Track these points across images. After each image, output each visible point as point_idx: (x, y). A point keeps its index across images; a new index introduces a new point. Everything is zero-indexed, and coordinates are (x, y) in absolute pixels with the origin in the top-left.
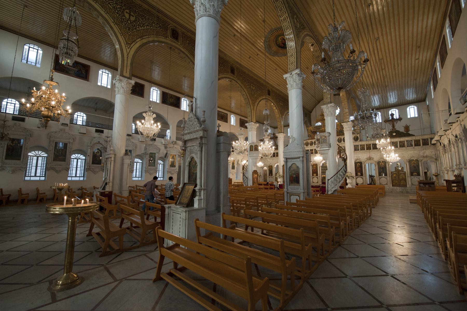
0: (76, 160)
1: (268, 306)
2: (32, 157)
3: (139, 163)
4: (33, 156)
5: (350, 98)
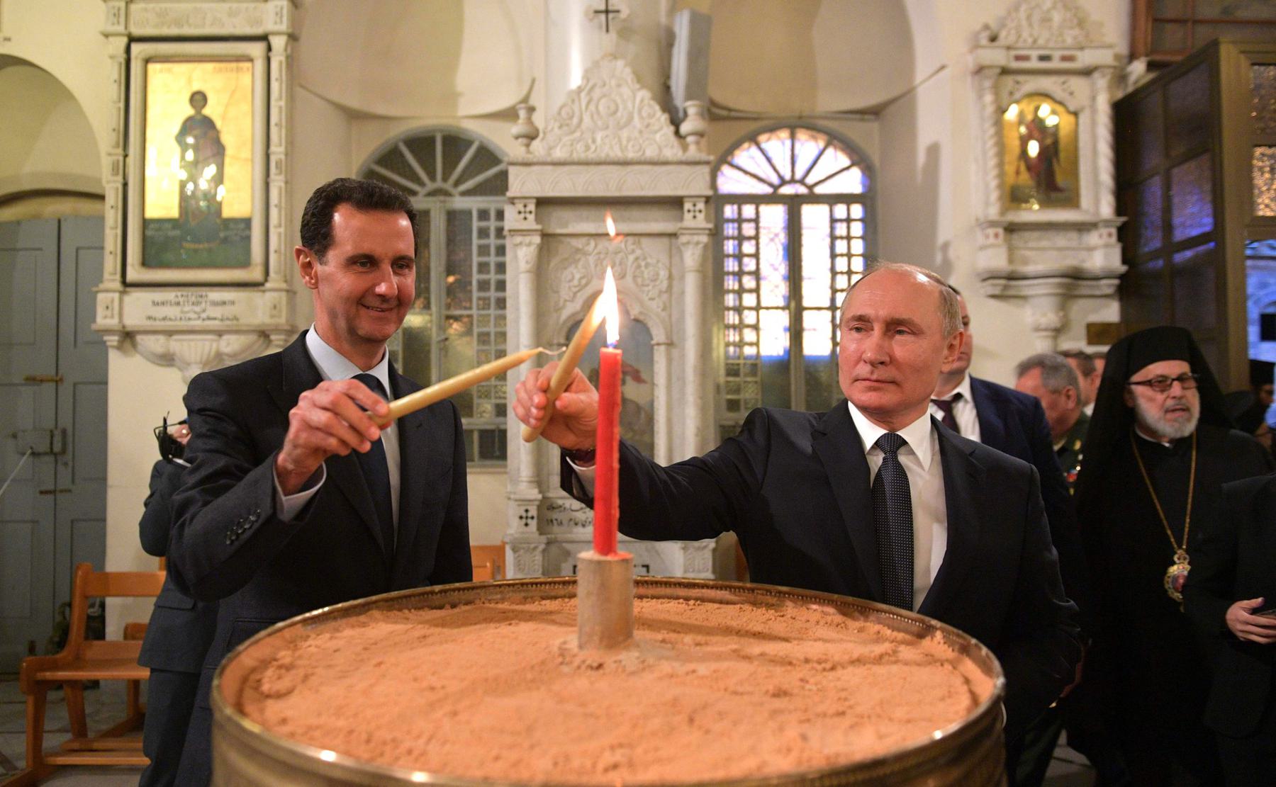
0: (774, 216)
1: (793, 388)
2: (748, 211)
3: (833, 200)
4: (757, 200)
5: (526, 568)
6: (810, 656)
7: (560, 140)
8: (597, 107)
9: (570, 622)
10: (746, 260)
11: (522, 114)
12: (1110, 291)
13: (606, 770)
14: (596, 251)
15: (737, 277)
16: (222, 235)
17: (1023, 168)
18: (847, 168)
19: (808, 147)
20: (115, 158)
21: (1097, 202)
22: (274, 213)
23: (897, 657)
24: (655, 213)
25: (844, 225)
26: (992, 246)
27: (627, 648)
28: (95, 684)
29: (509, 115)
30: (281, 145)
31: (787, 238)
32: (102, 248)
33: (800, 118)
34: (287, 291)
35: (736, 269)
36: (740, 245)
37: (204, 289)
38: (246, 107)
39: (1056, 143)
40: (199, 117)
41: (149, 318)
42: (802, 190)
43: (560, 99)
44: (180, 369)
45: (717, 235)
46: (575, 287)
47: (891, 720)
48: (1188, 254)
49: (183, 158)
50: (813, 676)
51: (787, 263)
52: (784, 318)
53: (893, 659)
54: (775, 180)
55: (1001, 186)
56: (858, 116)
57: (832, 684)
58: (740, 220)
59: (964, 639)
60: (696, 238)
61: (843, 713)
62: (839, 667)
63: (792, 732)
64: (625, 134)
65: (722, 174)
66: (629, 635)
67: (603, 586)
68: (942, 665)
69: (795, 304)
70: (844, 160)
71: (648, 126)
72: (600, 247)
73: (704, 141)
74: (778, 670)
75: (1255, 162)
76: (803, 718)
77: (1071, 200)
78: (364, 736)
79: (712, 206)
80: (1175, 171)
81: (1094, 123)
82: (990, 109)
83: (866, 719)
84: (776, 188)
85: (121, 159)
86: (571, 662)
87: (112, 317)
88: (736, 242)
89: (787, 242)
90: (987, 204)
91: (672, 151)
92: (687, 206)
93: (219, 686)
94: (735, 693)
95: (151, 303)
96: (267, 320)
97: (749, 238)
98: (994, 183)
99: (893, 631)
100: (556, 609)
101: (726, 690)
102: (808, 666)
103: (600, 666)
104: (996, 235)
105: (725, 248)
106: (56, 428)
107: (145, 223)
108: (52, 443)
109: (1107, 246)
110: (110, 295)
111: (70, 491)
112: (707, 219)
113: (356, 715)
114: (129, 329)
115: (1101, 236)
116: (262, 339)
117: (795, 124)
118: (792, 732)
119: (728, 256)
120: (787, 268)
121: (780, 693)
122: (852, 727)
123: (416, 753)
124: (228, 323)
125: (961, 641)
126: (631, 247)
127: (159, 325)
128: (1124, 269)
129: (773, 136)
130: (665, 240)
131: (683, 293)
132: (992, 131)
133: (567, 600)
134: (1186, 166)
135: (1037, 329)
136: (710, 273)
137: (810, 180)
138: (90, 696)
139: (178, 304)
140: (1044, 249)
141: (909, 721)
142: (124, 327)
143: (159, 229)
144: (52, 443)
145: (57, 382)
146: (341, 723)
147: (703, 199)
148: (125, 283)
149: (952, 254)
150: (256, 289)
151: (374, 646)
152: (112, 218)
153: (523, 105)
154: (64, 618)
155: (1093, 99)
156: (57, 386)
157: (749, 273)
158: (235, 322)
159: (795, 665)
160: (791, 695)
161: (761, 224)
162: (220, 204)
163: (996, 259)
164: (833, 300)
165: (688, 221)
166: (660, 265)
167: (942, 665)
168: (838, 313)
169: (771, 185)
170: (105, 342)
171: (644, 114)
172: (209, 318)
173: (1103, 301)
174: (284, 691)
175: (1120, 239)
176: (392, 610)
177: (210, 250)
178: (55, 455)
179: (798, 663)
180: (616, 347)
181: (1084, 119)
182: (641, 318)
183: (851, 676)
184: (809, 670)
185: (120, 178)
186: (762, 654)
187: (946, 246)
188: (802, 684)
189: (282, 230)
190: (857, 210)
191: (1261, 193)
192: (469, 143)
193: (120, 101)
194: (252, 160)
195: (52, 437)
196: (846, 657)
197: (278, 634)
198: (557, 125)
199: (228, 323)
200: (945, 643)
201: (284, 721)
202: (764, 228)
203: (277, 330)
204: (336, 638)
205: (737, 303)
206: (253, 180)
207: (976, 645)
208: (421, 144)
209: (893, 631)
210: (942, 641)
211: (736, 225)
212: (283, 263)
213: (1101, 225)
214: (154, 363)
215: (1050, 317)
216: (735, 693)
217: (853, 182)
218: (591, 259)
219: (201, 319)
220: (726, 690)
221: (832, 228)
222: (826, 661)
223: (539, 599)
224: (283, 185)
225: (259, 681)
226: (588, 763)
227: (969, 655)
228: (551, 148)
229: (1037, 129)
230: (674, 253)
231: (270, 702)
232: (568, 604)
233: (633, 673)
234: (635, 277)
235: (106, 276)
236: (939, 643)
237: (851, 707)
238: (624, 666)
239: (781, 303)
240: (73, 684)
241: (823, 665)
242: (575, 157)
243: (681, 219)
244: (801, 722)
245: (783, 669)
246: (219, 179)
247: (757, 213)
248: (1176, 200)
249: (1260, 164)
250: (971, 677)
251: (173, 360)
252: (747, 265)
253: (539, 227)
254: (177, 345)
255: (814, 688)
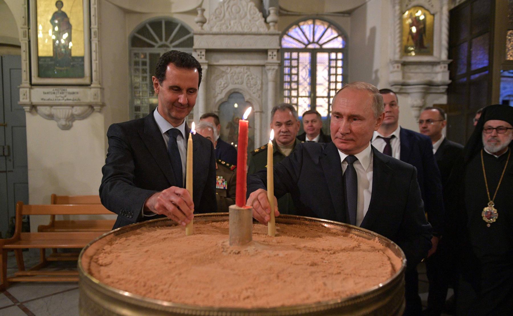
0: (305, 57)
2: (295, 55)
3: (330, 51)
4: (298, 50)
6: (325, 248)
7: (216, 24)
8: (231, 9)
9: (225, 232)
10: (293, 76)
11: (199, 12)
12: (444, 91)
13: (244, 299)
14: (230, 73)
15: (289, 84)
16: (72, 64)
17: (410, 37)
18: (337, 37)
19: (320, 28)
20: (25, 29)
21: (440, 53)
22: (94, 54)
23: (360, 248)
24: (256, 56)
25: (334, 62)
26: (396, 71)
27: (250, 245)
28: (27, 250)
29: (194, 12)
30: (96, 25)
31: (311, 67)
32: (21, 69)
33: (317, 15)
34: (101, 88)
35: (289, 80)
36: (291, 70)
37: (65, 87)
38: (80, 8)
39: (424, 28)
40: (60, 12)
41: (42, 99)
42: (317, 46)
43: (216, 6)
44: (57, 121)
45: (281, 66)
46: (222, 87)
47: (359, 276)
48: (477, 76)
49: (54, 30)
50: (326, 256)
51: (311, 78)
52: (308, 101)
53: (358, 249)
54: (306, 41)
55: (401, 46)
56: (342, 15)
57: (334, 260)
58: (291, 59)
59: (388, 241)
60: (273, 67)
61: (340, 273)
62: (337, 252)
63: (320, 282)
64: (243, 21)
65: (284, 39)
66: (250, 239)
67: (240, 220)
68: (379, 252)
69: (313, 96)
70: (335, 34)
71: (253, 18)
72: (232, 71)
73: (277, 25)
74: (312, 254)
75: (507, 37)
76: (324, 275)
77: (430, 52)
78: (143, 284)
79: (280, 53)
80: (474, 40)
81: (441, 19)
82: (398, 12)
83: (349, 276)
84: (306, 45)
85: (27, 30)
86: (227, 251)
87: (27, 99)
88: (289, 69)
89: (311, 69)
90: (395, 53)
91: (263, 29)
92: (270, 53)
93: (81, 262)
94: (295, 264)
95: (43, 93)
96: (92, 100)
97: (295, 67)
98: (398, 45)
99: (357, 236)
100: (219, 226)
101: (291, 263)
102: (324, 252)
103: (239, 253)
104: (398, 67)
105: (285, 71)
106: (5, 145)
107: (39, 58)
108: (4, 152)
109: (443, 72)
110: (25, 89)
111: (12, 171)
112: (278, 59)
113: (138, 274)
114: (34, 104)
115: (441, 68)
116: (90, 109)
117: (315, 18)
118: (320, 282)
119: (286, 74)
120: (310, 80)
121: (313, 264)
122: (344, 279)
123: (165, 291)
124: (75, 101)
125: (386, 242)
126: (245, 71)
127: (46, 102)
128: (450, 82)
129: (306, 23)
130: (260, 68)
131: (267, 91)
132: (398, 22)
133: (223, 222)
134: (479, 38)
135: (413, 106)
136: (279, 82)
137: (321, 42)
138: (25, 254)
139: (54, 93)
140: (416, 73)
141: (367, 277)
142: (32, 103)
143: (45, 61)
144: (4, 152)
145: (4, 126)
146: (133, 278)
147: (276, 50)
148: (32, 85)
149: (379, 74)
150: (87, 87)
151: (144, 243)
152: (24, 56)
153: (199, 8)
154: (13, 223)
155: (441, 8)
156: (4, 127)
157: (294, 82)
158: (79, 101)
159: (319, 252)
160: (318, 265)
161: (300, 61)
162: (70, 50)
163: (397, 77)
164: (329, 93)
165: (270, 60)
166: (258, 78)
167: (379, 252)
168: (331, 99)
169: (304, 44)
170: (24, 109)
171: (252, 12)
172: (68, 100)
173: (441, 95)
174: (109, 263)
175: (449, 69)
176: (151, 227)
177: (67, 70)
178: (6, 156)
179: (320, 251)
180: (246, 120)
181: (437, 17)
182: (250, 101)
183: (342, 256)
184: (325, 254)
185: (27, 39)
186: (305, 247)
187: (377, 71)
188: (322, 260)
189: (97, 62)
190: (340, 56)
191: (509, 50)
192: (176, 24)
193: (25, 5)
194: (84, 31)
195: (4, 149)
196: (339, 248)
197: (105, 238)
198: (214, 17)
199: (75, 101)
200: (379, 242)
201: (109, 277)
202: (301, 63)
203: (97, 105)
204: (128, 239)
205: (289, 94)
206: (84, 40)
207: (393, 244)
208: (156, 24)
209: (357, 236)
210: (378, 241)
211: (289, 61)
212: (98, 76)
213: (441, 62)
214: (46, 118)
215: (418, 102)
216: (295, 264)
217: (338, 43)
218: (229, 76)
219: (64, 100)
220: (291, 263)
221: (329, 63)
222: (331, 250)
223: (211, 222)
224: (97, 42)
225: (97, 259)
226: (237, 296)
227: (389, 247)
228: (212, 27)
229: (416, 22)
230: (264, 73)
231: (102, 268)
232: (223, 224)
233: (253, 255)
234: (247, 84)
235: (23, 81)
236: (377, 242)
237: (343, 270)
238: (249, 253)
239: (307, 95)
240: (18, 249)
241: (330, 252)
242: (222, 31)
243: (267, 59)
244: (323, 277)
245: (314, 253)
246: (69, 39)
247: (298, 56)
248: (473, 53)
249: (510, 38)
250: (391, 257)
251: (53, 117)
252: (293, 78)
253: (207, 62)
254: (54, 111)
255: (327, 262)
